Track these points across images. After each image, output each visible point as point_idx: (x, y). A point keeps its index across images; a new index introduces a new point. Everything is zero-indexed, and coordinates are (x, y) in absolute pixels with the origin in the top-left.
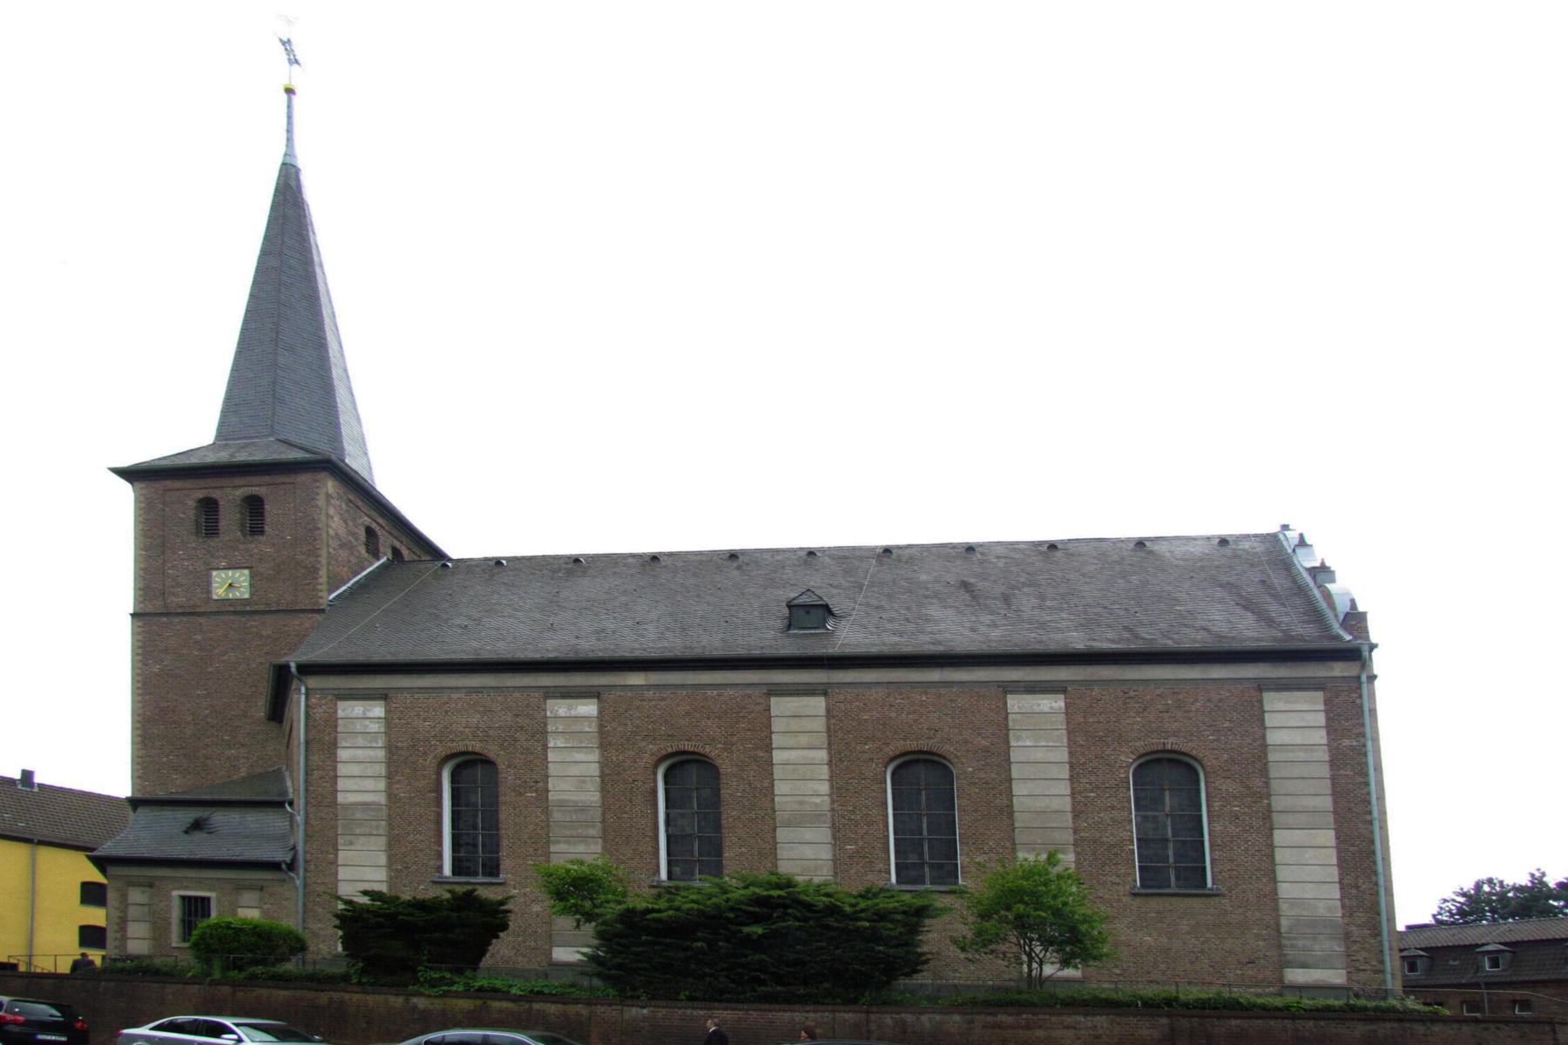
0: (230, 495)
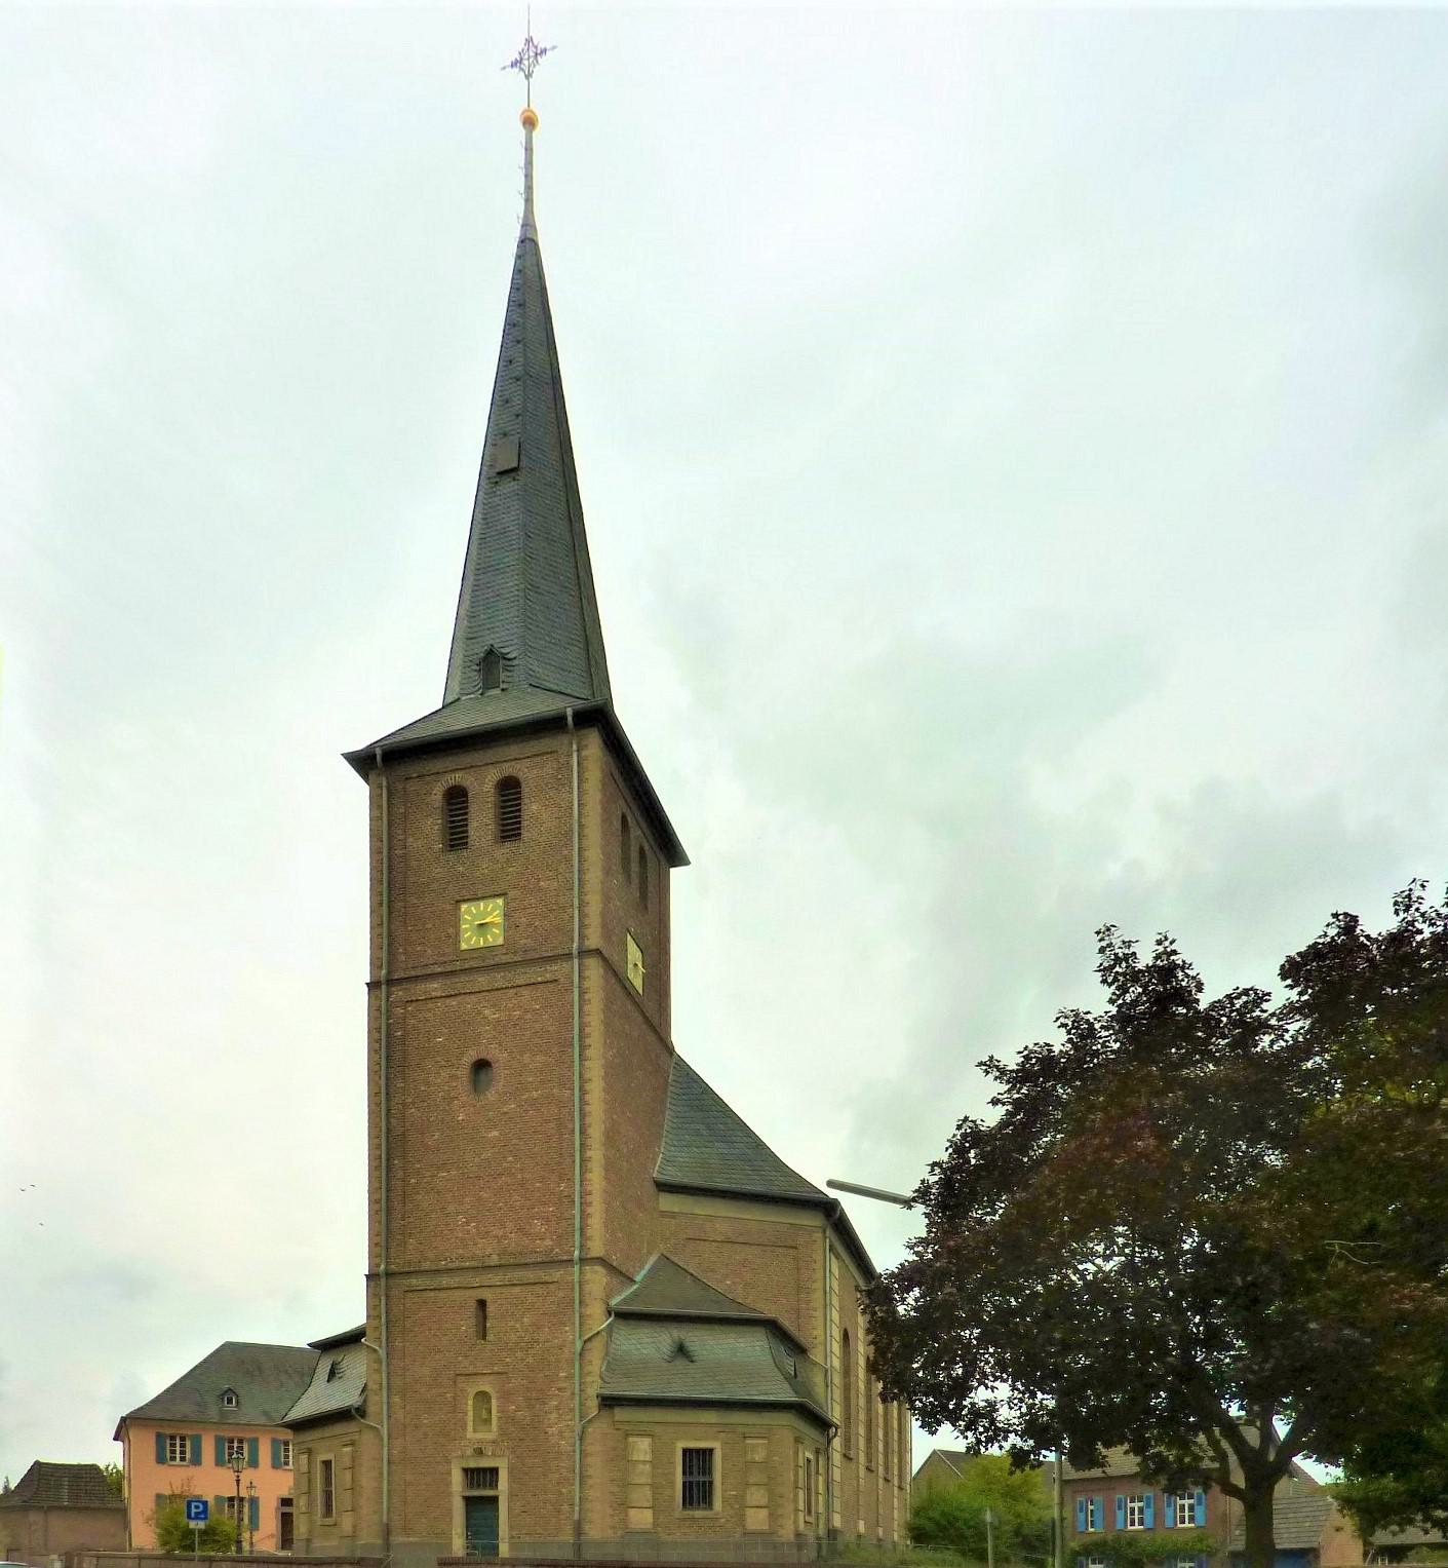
0: (481, 781)
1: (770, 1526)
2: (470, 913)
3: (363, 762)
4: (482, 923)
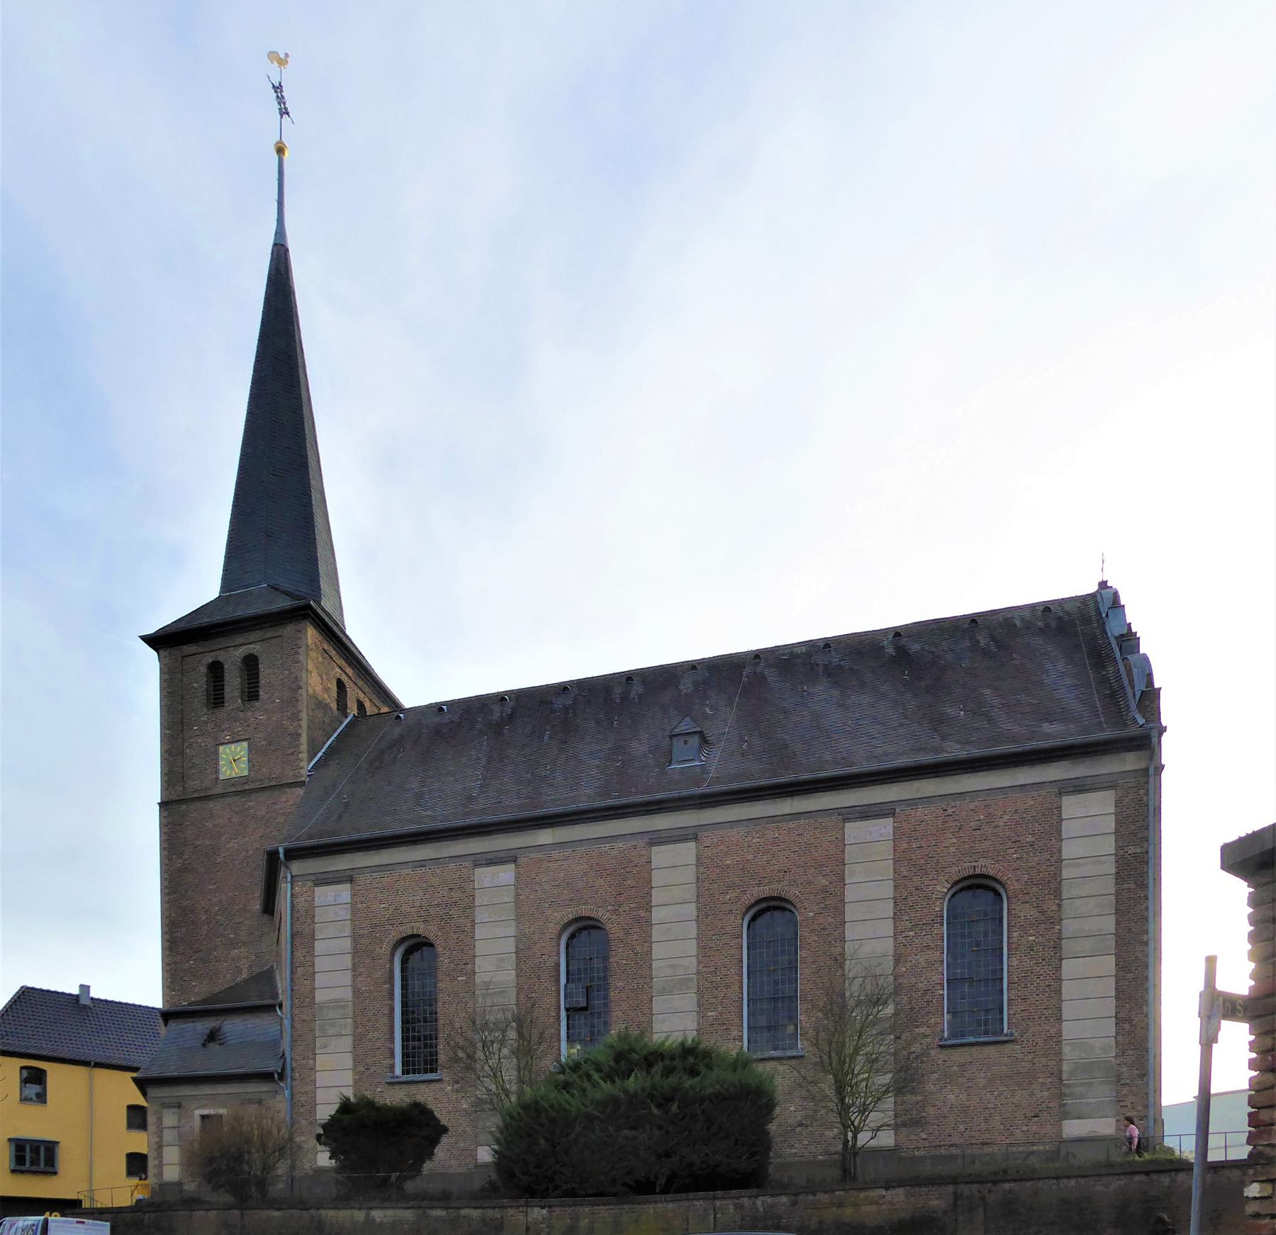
0: (232, 655)
1: (841, 844)
2: (226, 752)
3: (154, 641)
4: (233, 761)
